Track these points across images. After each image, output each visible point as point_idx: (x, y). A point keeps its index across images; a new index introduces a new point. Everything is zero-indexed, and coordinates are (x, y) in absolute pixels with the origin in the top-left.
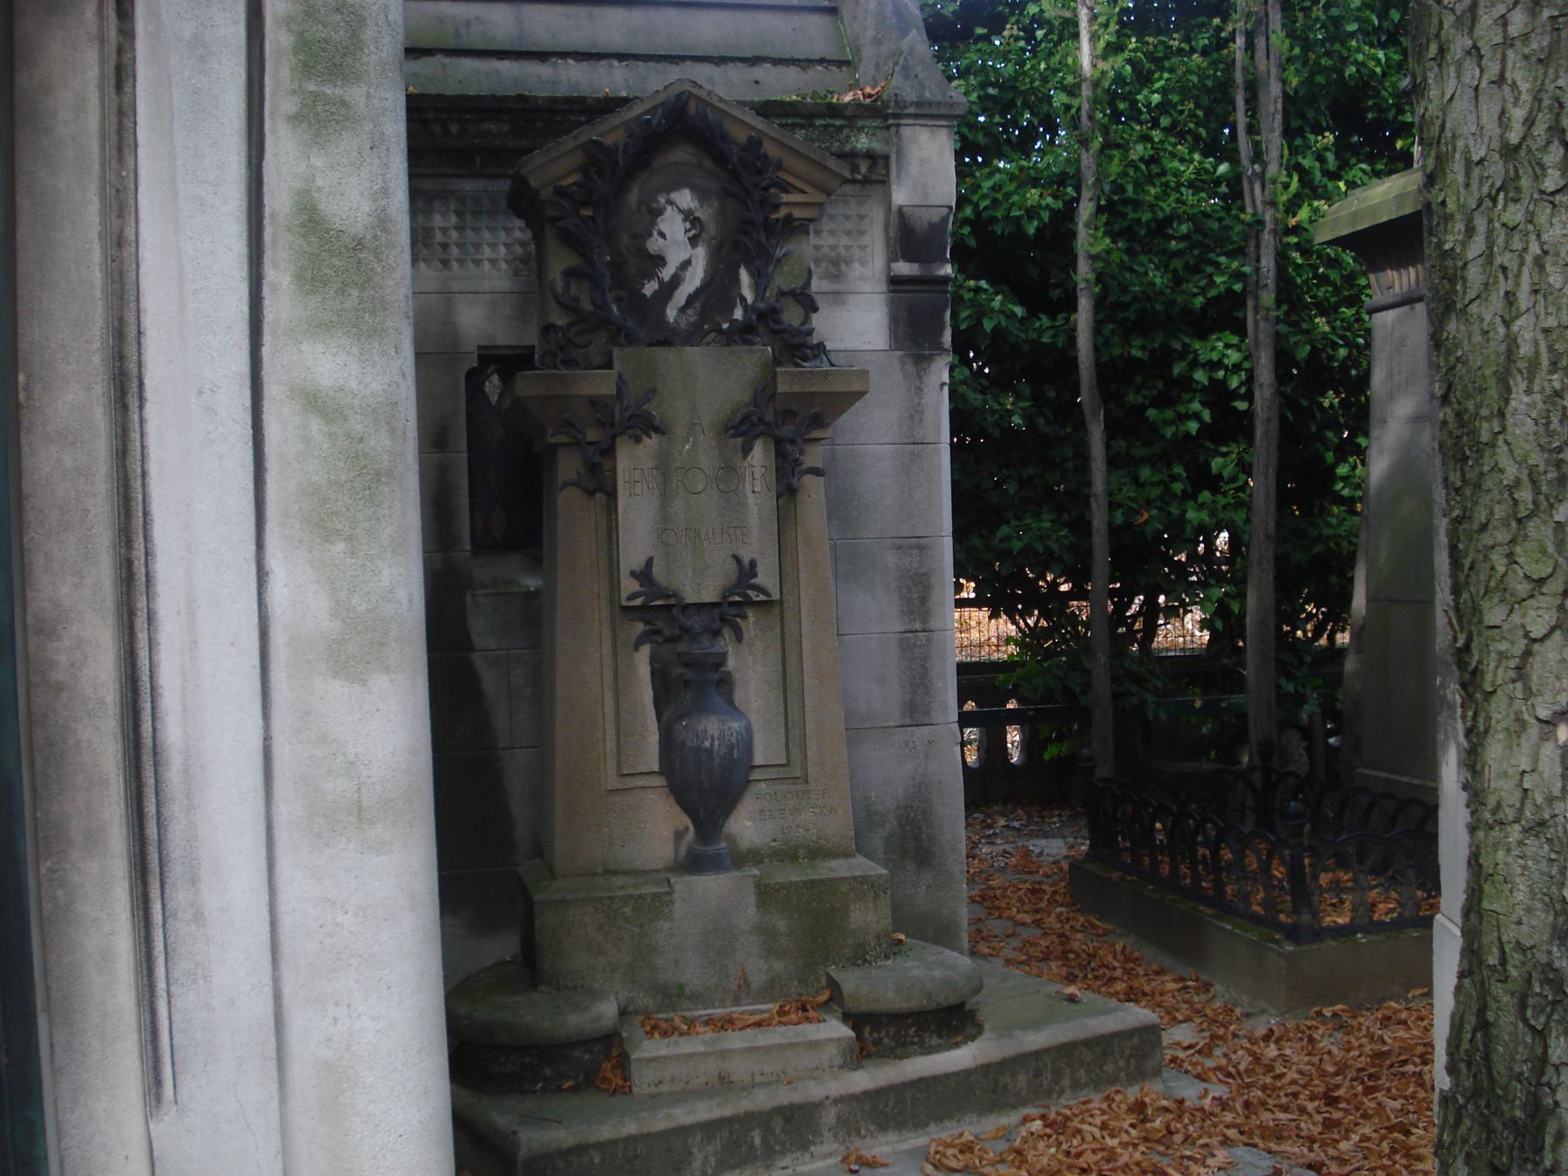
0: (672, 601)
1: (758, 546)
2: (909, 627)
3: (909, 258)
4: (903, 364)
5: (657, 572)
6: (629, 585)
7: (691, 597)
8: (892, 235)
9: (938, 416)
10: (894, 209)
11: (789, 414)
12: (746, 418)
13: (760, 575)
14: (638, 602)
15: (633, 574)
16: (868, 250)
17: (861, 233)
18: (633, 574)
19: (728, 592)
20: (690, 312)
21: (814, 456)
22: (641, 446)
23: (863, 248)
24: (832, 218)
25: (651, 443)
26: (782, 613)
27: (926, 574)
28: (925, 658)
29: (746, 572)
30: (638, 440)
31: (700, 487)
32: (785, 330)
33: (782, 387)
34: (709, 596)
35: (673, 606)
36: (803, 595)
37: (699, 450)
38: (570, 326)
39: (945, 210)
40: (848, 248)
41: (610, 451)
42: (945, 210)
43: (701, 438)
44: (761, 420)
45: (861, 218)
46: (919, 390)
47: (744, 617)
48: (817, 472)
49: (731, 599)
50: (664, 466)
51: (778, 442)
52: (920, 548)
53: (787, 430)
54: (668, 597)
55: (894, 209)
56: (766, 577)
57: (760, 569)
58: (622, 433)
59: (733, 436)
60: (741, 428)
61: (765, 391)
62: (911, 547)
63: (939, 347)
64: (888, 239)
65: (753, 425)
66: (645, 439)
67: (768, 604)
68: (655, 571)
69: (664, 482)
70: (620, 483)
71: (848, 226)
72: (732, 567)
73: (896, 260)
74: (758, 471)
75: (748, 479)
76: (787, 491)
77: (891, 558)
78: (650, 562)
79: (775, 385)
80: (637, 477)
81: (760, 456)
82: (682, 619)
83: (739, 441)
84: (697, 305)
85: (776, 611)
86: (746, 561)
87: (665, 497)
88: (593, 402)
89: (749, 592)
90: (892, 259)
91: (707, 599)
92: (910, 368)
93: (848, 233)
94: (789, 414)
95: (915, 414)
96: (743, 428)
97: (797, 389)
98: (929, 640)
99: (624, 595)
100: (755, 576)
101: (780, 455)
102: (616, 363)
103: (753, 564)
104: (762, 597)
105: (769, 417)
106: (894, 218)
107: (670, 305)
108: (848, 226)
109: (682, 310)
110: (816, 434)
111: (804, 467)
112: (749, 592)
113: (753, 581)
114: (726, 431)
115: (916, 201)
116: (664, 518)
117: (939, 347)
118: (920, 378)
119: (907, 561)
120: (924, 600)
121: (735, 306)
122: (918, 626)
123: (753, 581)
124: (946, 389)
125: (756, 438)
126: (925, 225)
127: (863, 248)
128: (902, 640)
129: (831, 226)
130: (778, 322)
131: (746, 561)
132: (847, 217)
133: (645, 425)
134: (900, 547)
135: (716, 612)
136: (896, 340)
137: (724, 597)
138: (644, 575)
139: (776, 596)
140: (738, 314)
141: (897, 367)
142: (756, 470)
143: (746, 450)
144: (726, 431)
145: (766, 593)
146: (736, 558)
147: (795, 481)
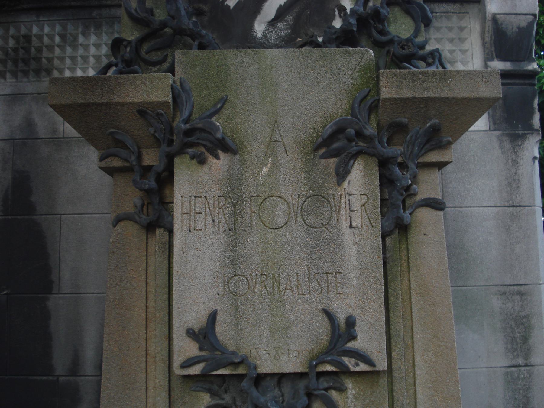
0: (241, 370)
1: (357, 298)
2: (514, 362)
3: (502, 58)
4: (501, 141)
5: (223, 331)
6: (186, 348)
7: (267, 365)
8: (487, 39)
9: (532, 184)
10: (489, 16)
11: (397, 129)
12: (339, 131)
13: (360, 336)
14: (196, 370)
15: (191, 333)
16: (469, 53)
17: (462, 40)
18: (191, 333)
19: (317, 358)
20: (280, 25)
21: (428, 186)
22: (206, 168)
23: (464, 52)
24: (438, 29)
25: (219, 164)
26: (391, 383)
27: (527, 317)
28: (527, 389)
29: (342, 333)
30: (202, 162)
31: (281, 221)
32: (391, 42)
33: (387, 92)
34: (291, 364)
35: (241, 377)
36: (418, 358)
37: (279, 171)
38: (141, 41)
39: (531, 18)
40: (452, 52)
41: (166, 178)
42: (531, 18)
43: (283, 158)
44: (359, 135)
45: (461, 29)
46: (515, 162)
47: (341, 390)
48: (436, 205)
49: (321, 369)
50: (234, 195)
51: (384, 163)
52: (521, 294)
53: (396, 150)
54: (236, 365)
55: (489, 16)
56: (369, 339)
57: (360, 329)
58: (181, 152)
59: (323, 157)
60: (337, 144)
61: (367, 101)
62: (513, 294)
63: (530, 128)
64: (484, 44)
65: (350, 140)
66: (211, 159)
67: (372, 375)
68: (219, 329)
69: (235, 214)
70: (177, 214)
71: (451, 35)
72: (323, 328)
73: (492, 60)
74: (357, 201)
75: (344, 212)
76: (396, 228)
77: (496, 303)
78: (213, 317)
79: (378, 93)
80: (199, 206)
81: (360, 179)
82: (254, 393)
83: (332, 162)
84: (290, 18)
85: (384, 381)
86: (341, 317)
87: (235, 234)
88: (143, 111)
89: (346, 360)
90: (488, 58)
91: (288, 369)
92: (507, 145)
93: (451, 41)
94: (397, 129)
95: (513, 182)
96: (336, 145)
97: (407, 93)
98: (530, 374)
99: (177, 360)
100: (354, 338)
101: (387, 181)
102: (178, 69)
103: (351, 322)
104: (363, 367)
105: (371, 130)
106: (489, 25)
107: (258, 19)
108: (451, 35)
109: (272, 23)
110: (434, 157)
111: (418, 198)
112: (346, 360)
113: (351, 345)
114: (316, 149)
115: (506, 10)
116: (234, 261)
117: (530, 128)
118: (516, 153)
119: (510, 305)
120: (525, 339)
121: (334, 18)
122: (521, 361)
123: (351, 345)
124: (537, 162)
125: (355, 156)
126: (515, 29)
127: (464, 52)
128: (507, 374)
129: (438, 35)
130: (382, 32)
131: (341, 317)
132: (450, 29)
133: (206, 141)
134: (504, 293)
135: (302, 385)
136: (494, 123)
137: (312, 367)
138: (205, 335)
139: (382, 366)
140: (337, 23)
141: (496, 144)
142: (353, 199)
143: (342, 174)
144: (316, 149)
145: (368, 361)
146: (327, 313)
147: (406, 215)
